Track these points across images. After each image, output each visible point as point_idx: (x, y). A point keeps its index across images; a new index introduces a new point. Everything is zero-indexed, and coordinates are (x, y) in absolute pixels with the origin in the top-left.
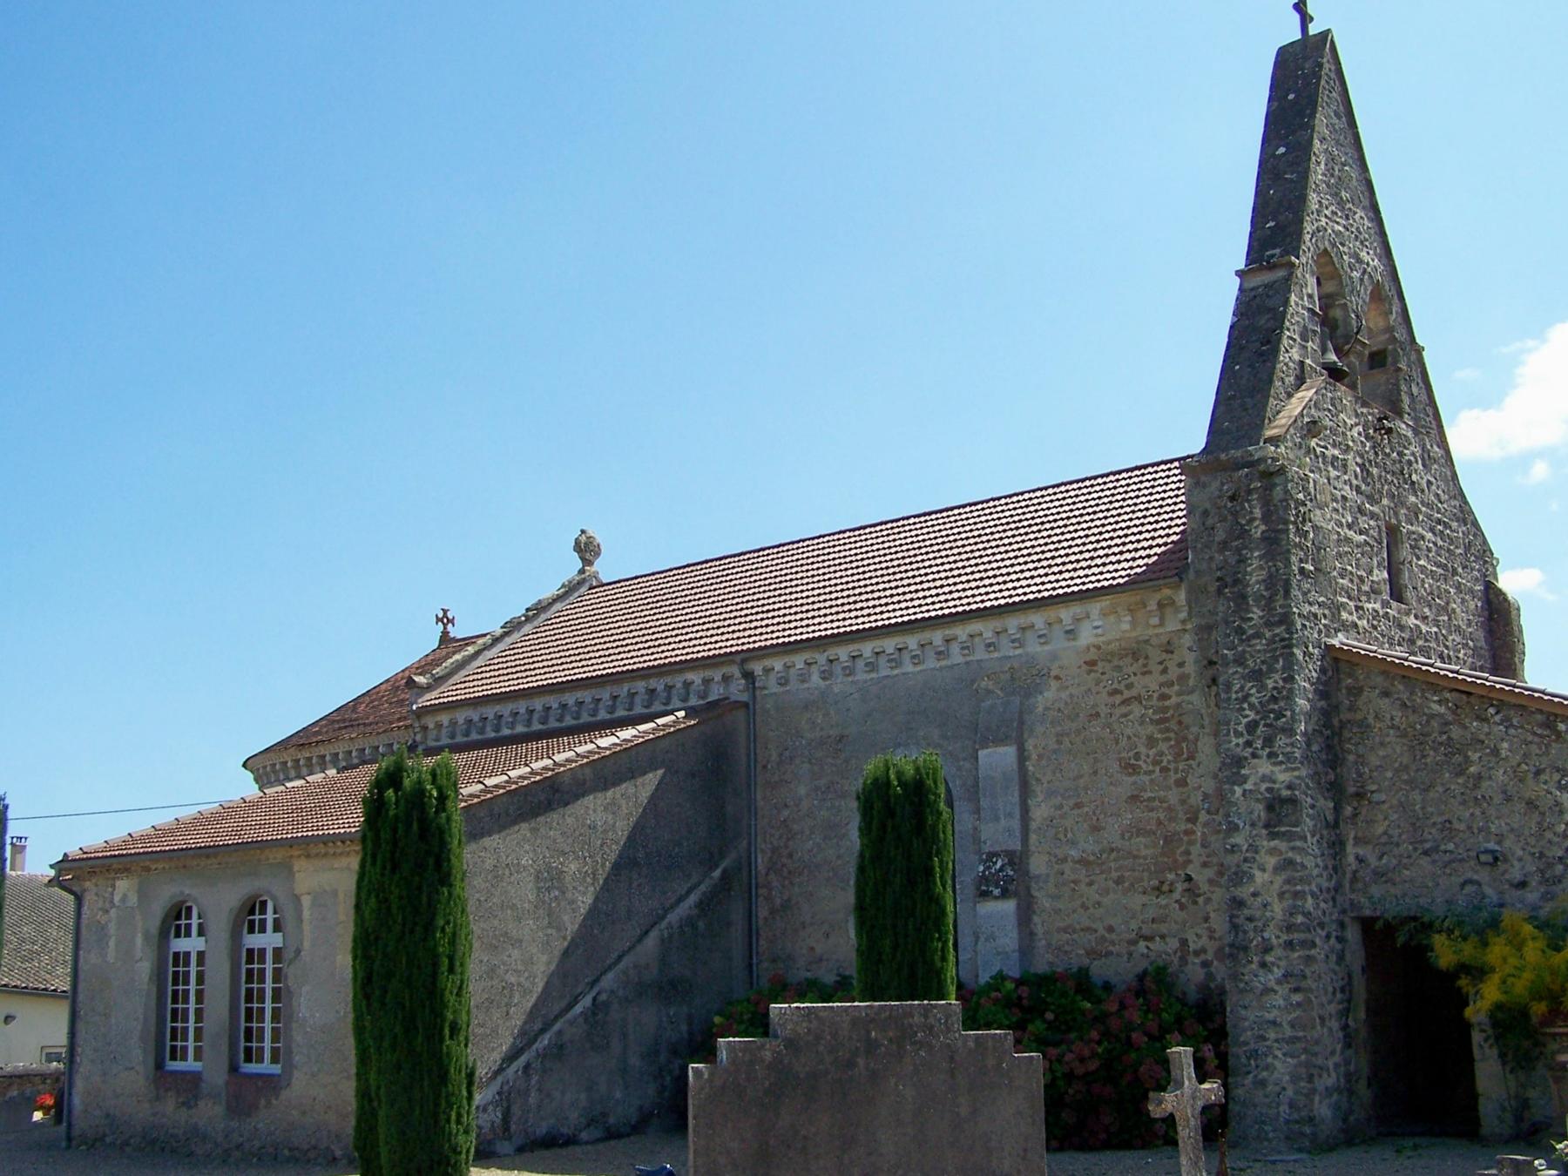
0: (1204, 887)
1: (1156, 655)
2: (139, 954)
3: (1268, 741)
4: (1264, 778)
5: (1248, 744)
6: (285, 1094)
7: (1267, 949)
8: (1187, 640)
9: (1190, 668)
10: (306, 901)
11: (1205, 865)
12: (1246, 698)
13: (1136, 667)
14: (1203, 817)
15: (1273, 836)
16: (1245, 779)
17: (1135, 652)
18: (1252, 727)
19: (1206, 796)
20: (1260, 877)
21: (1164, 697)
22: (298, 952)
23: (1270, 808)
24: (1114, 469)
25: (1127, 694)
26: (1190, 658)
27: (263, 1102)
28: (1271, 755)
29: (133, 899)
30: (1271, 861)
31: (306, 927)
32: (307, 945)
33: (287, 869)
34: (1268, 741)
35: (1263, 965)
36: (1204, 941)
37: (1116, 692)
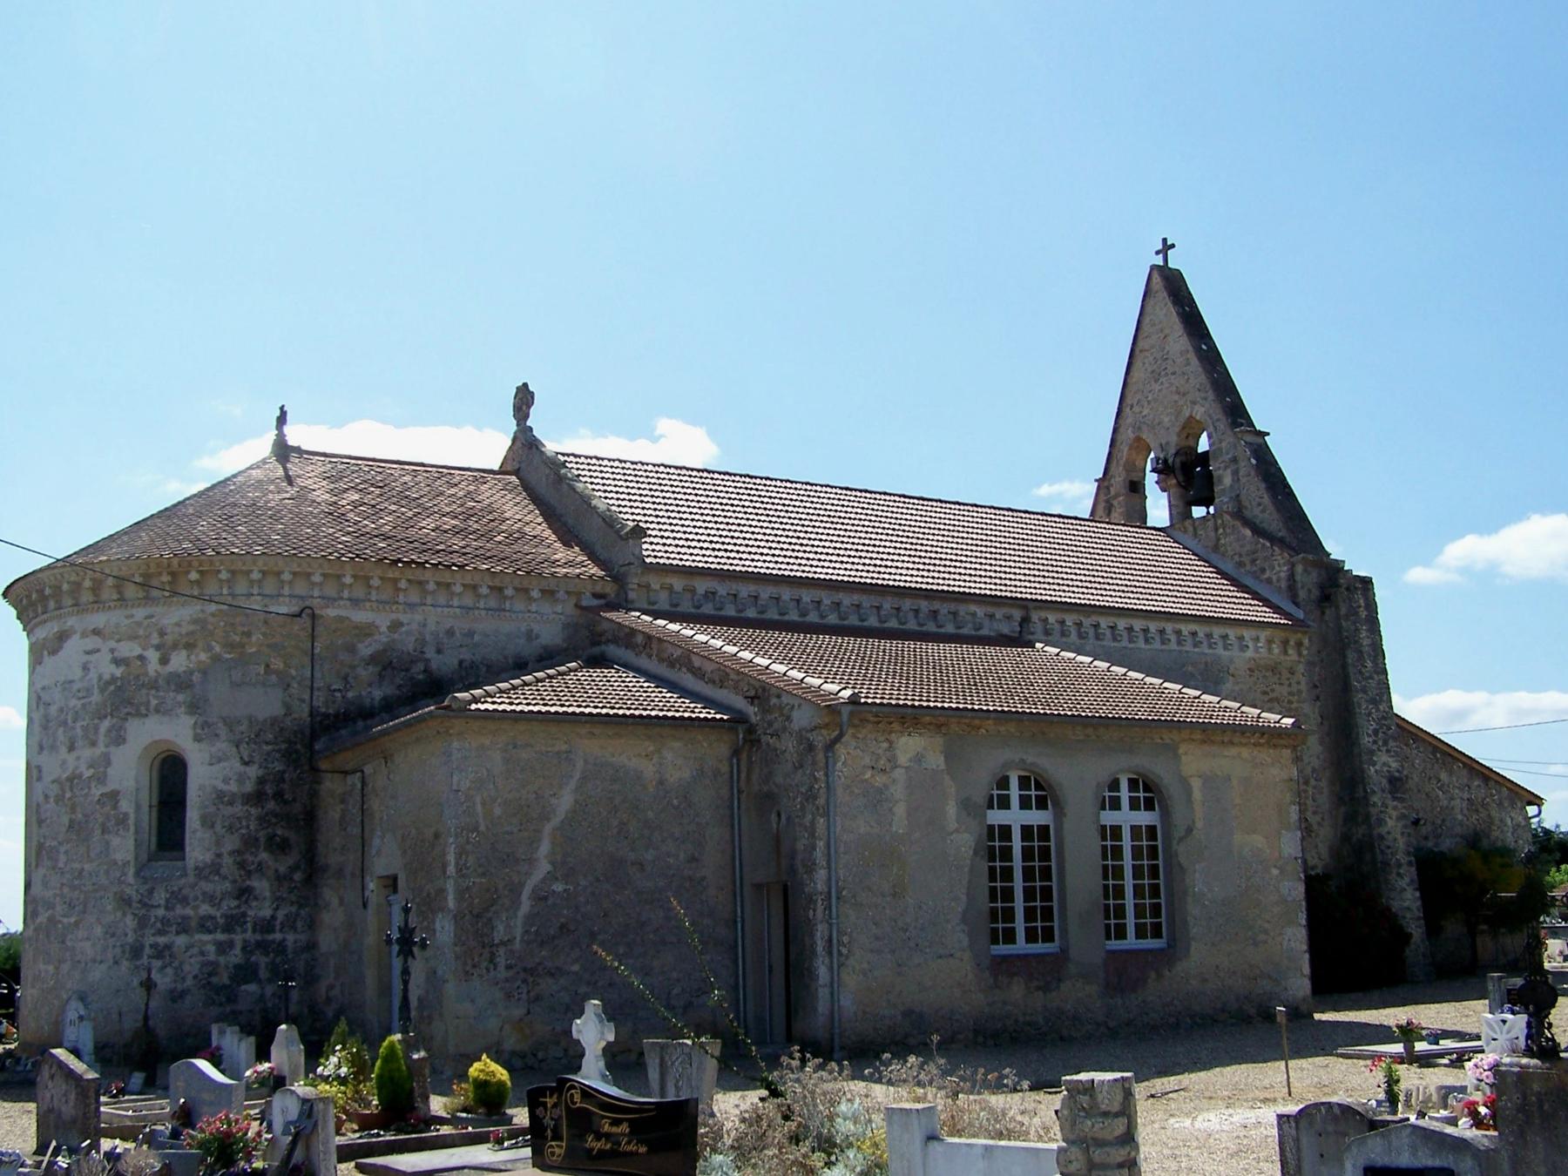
0: (1315, 827)
1: (1286, 674)
2: (952, 825)
3: (1385, 743)
4: (1384, 764)
5: (1375, 742)
6: (1180, 967)
7: (1399, 865)
8: (1301, 668)
9: (1303, 687)
10: (1196, 784)
11: (1315, 813)
12: (1370, 714)
13: (1275, 679)
14: (1313, 782)
15: (1395, 799)
16: (1374, 764)
17: (1274, 669)
18: (1376, 732)
19: (1314, 770)
20: (1390, 823)
21: (1290, 702)
22: (1189, 830)
23: (1390, 782)
24: (328, 451)
25: (1272, 695)
26: (1303, 681)
27: (1153, 975)
28: (1388, 751)
29: (936, 761)
30: (1394, 814)
31: (1198, 807)
32: (1199, 824)
33: (1172, 750)
34: (1385, 743)
35: (1399, 874)
36: (1316, 861)
37: (1265, 693)
